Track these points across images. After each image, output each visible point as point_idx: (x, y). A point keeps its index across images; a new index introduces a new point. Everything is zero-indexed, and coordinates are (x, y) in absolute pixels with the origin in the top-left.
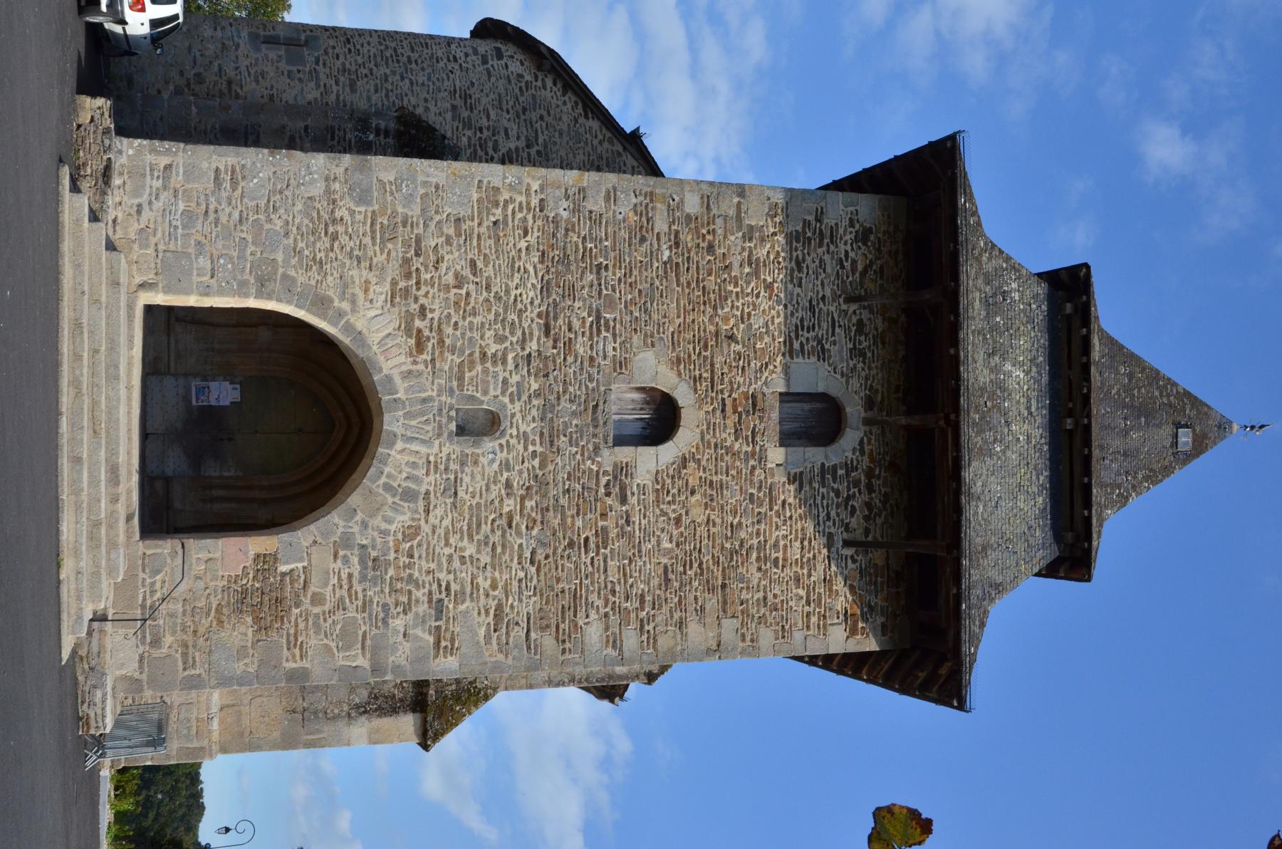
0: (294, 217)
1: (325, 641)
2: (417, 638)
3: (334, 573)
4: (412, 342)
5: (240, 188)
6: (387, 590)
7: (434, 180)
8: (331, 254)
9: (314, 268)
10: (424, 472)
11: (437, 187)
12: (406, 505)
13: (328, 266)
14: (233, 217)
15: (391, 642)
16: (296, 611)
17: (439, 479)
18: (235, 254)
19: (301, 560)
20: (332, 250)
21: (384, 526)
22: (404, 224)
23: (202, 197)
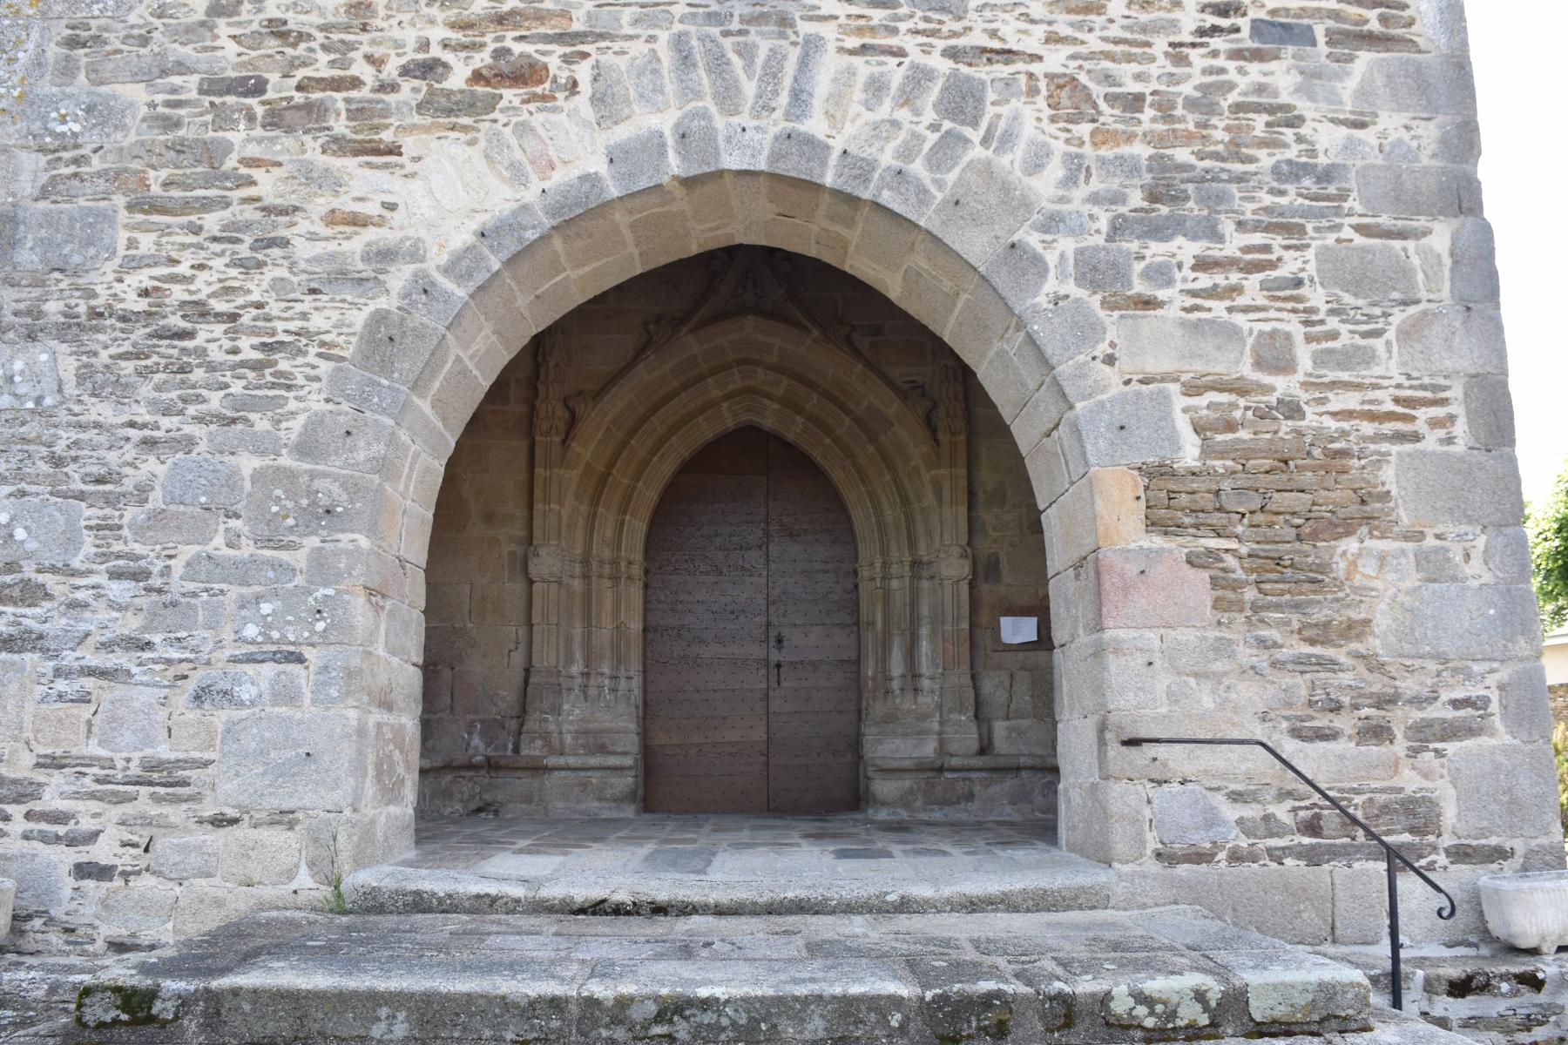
0: (132, 424)
1: (1391, 334)
2: (1364, 93)
3: (1196, 308)
4: (510, 95)
5: (41, 578)
6: (1238, 167)
7: (53, 51)
8: (246, 319)
9: (284, 365)
10: (892, 61)
11: (73, 43)
12: (990, 111)
13: (280, 326)
14: (124, 599)
15: (1379, 161)
16: (1311, 419)
17: (910, 24)
18: (234, 591)
19: (1165, 398)
20: (233, 317)
21: (1055, 170)
22: (174, 124)
23: (61, 685)
